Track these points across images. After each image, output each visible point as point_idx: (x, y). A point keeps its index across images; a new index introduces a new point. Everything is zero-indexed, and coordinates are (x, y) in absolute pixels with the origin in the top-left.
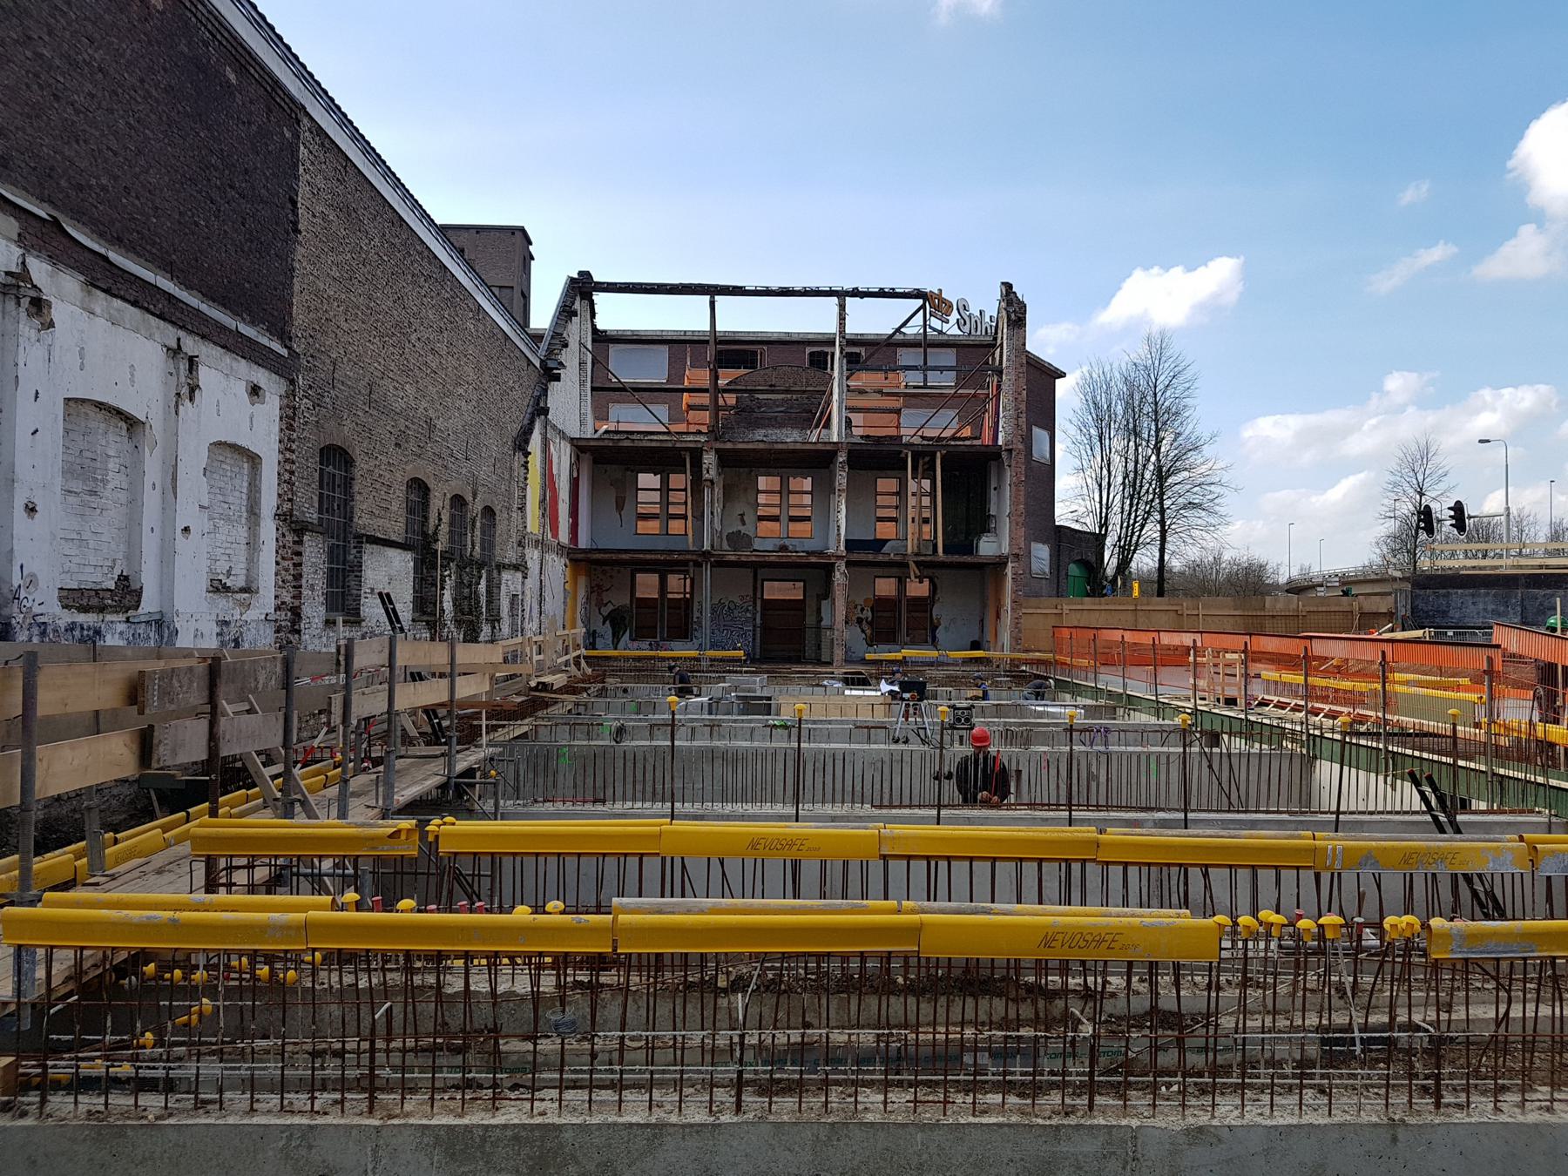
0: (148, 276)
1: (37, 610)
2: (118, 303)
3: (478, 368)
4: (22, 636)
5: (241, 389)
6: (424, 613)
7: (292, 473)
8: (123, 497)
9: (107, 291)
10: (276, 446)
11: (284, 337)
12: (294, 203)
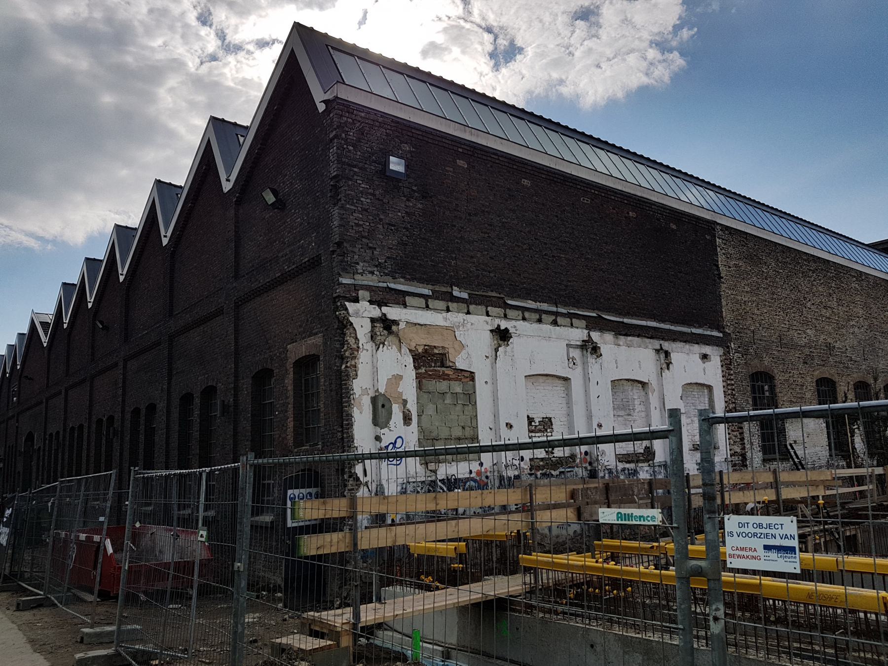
0: (643, 323)
1: (606, 464)
2: (629, 338)
3: (866, 306)
4: (601, 474)
5: (697, 358)
6: (843, 451)
7: (733, 390)
8: (643, 414)
9: (624, 335)
10: (721, 379)
11: (720, 328)
12: (717, 266)
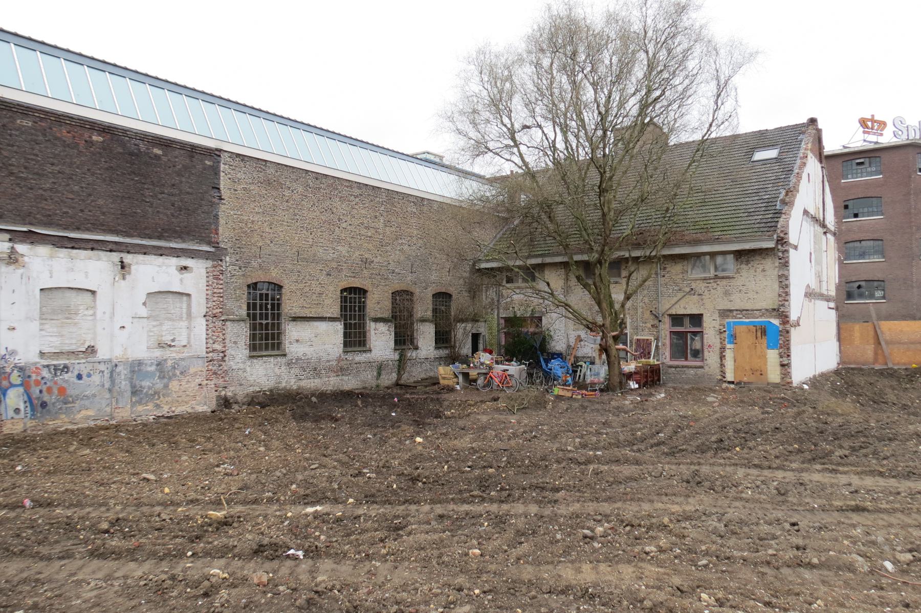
5: (173, 271)
